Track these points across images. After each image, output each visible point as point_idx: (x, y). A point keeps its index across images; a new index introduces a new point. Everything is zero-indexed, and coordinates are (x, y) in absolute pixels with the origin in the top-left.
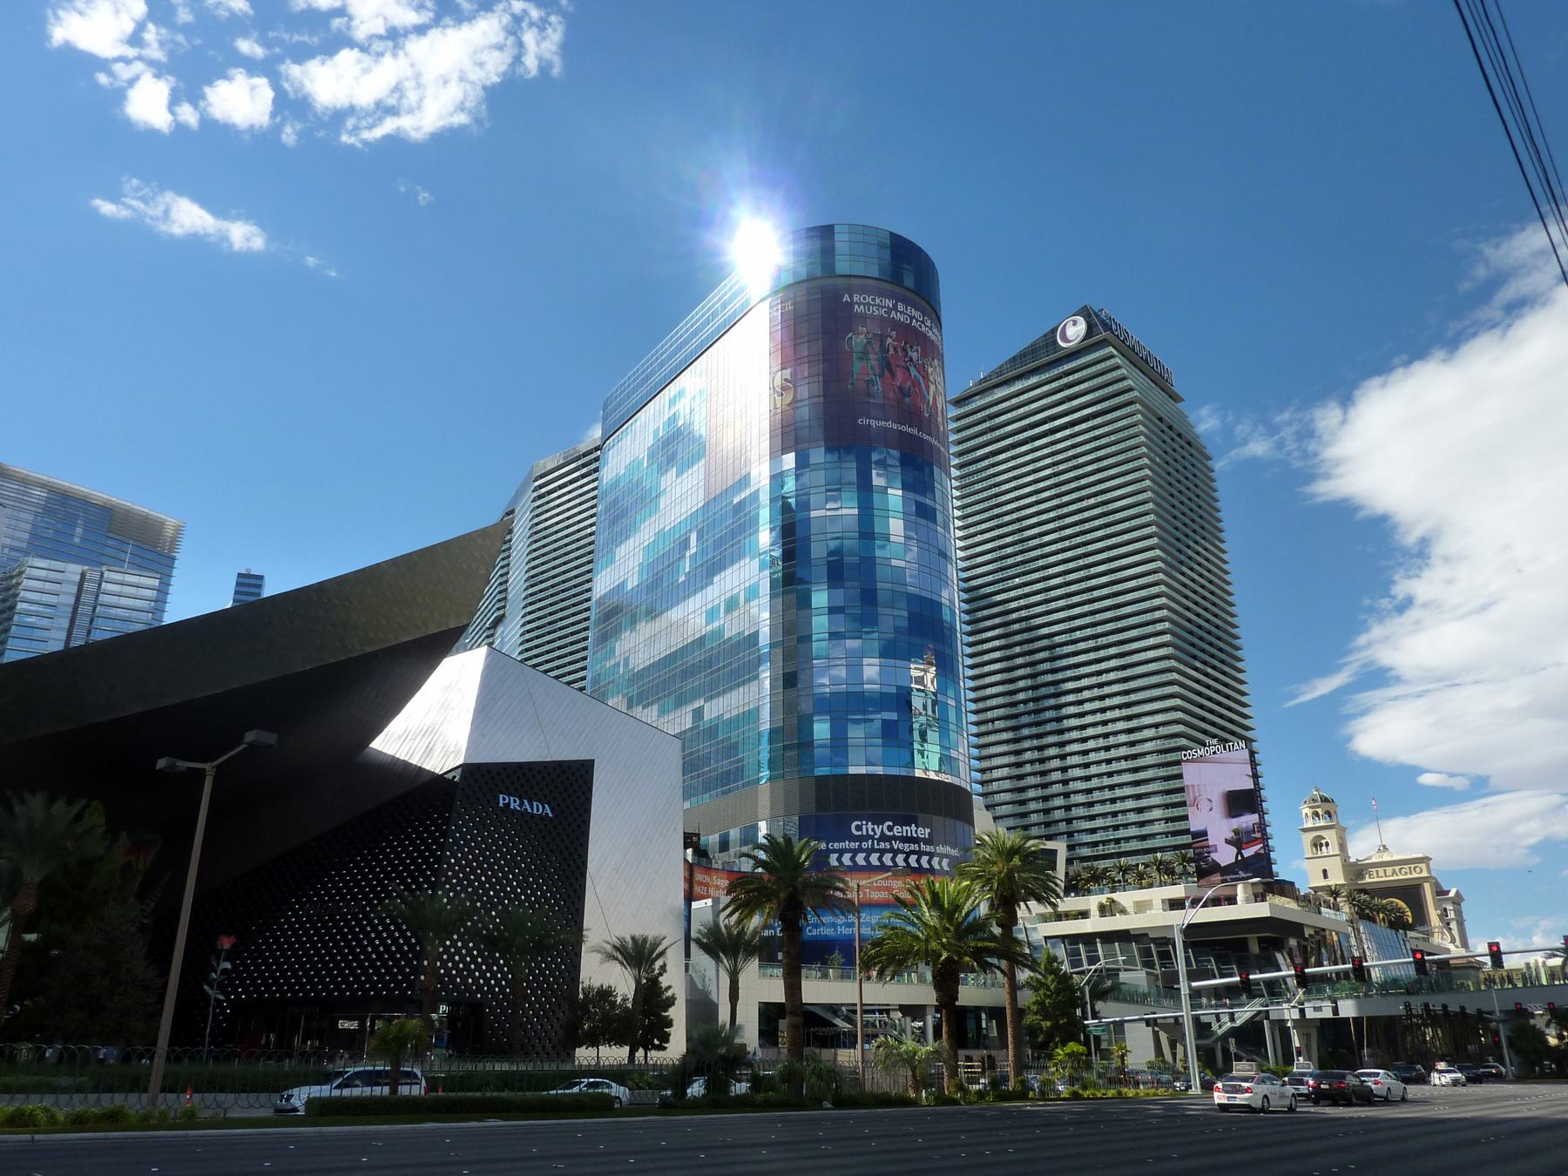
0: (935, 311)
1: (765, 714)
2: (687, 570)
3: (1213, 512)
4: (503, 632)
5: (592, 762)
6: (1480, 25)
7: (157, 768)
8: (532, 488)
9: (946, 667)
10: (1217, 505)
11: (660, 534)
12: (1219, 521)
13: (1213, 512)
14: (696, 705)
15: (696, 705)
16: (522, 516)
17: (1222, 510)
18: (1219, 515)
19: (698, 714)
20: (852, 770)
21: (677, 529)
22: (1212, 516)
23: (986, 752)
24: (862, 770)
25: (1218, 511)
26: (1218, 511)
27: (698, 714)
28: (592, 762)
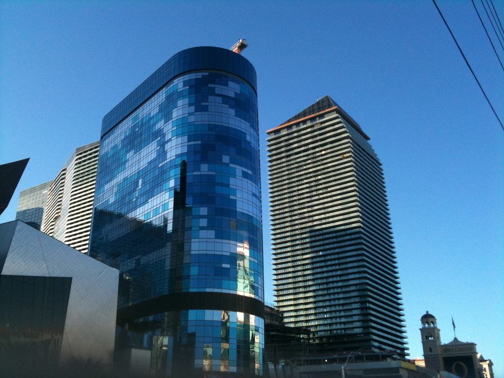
0: (254, 89)
1: (168, 263)
2: (137, 196)
3: (386, 215)
4: (59, 224)
5: (71, 278)
6: (491, 7)
7: (422, 364)
8: (75, 159)
9: (256, 246)
10: (385, 189)
11: (125, 179)
12: (384, 187)
13: (384, 197)
14: (137, 257)
15: (137, 257)
16: (70, 172)
17: (396, 247)
18: (386, 198)
19: (138, 261)
20: (191, 290)
21: (159, 192)
22: (382, 185)
23: (281, 293)
24: (195, 290)
25: (383, 179)
26: (383, 179)
27: (138, 261)
28: (71, 278)
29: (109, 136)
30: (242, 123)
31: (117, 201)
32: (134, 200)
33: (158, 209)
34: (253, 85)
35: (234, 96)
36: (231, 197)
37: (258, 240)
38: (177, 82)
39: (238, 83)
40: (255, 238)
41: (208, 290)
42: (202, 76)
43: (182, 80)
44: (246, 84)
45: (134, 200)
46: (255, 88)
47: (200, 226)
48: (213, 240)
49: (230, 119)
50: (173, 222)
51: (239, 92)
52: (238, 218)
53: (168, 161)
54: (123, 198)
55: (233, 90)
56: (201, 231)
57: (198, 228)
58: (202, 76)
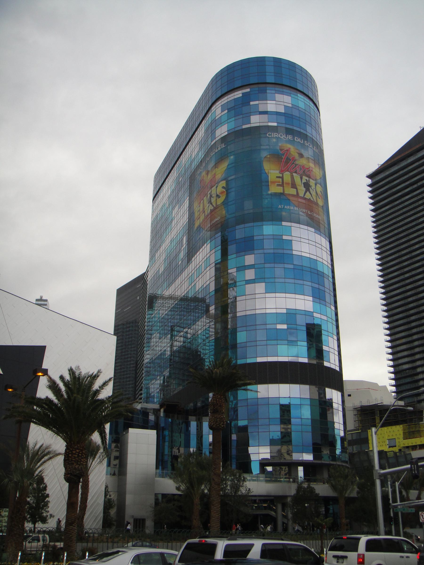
29: (158, 197)
30: (299, 101)
31: (166, 269)
32: (180, 263)
33: (201, 267)
34: (311, 96)
35: (283, 111)
36: (285, 237)
37: (326, 290)
38: (215, 109)
39: (289, 94)
40: (321, 288)
41: (259, 360)
42: (243, 93)
43: (220, 105)
44: (300, 95)
45: (180, 263)
46: (317, 105)
47: (260, 111)
48: (263, 296)
49: (282, 68)
50: (222, 249)
51: (290, 105)
52: (295, 263)
53: (217, 139)
54: (170, 264)
55: (282, 103)
56: (247, 286)
57: (244, 283)
58: (243, 93)
